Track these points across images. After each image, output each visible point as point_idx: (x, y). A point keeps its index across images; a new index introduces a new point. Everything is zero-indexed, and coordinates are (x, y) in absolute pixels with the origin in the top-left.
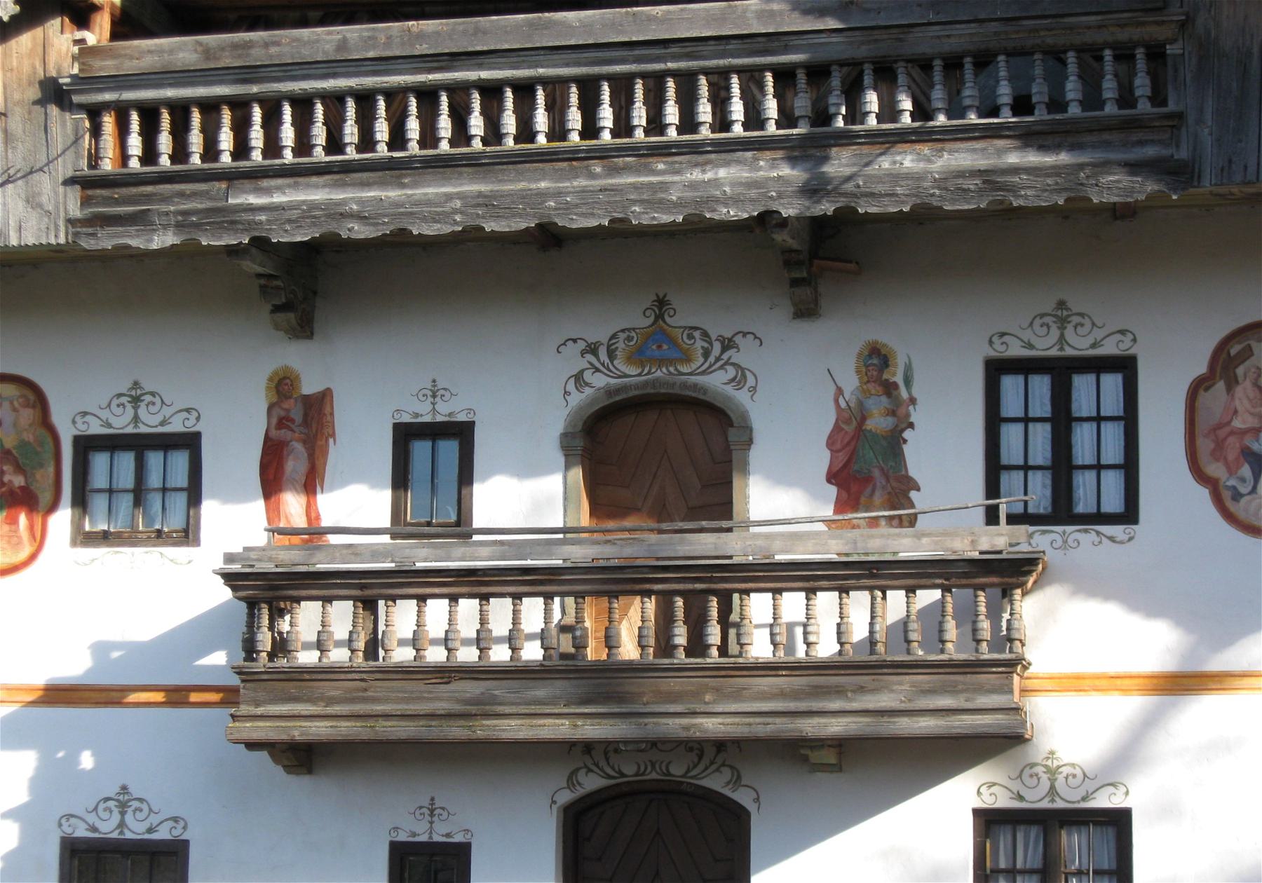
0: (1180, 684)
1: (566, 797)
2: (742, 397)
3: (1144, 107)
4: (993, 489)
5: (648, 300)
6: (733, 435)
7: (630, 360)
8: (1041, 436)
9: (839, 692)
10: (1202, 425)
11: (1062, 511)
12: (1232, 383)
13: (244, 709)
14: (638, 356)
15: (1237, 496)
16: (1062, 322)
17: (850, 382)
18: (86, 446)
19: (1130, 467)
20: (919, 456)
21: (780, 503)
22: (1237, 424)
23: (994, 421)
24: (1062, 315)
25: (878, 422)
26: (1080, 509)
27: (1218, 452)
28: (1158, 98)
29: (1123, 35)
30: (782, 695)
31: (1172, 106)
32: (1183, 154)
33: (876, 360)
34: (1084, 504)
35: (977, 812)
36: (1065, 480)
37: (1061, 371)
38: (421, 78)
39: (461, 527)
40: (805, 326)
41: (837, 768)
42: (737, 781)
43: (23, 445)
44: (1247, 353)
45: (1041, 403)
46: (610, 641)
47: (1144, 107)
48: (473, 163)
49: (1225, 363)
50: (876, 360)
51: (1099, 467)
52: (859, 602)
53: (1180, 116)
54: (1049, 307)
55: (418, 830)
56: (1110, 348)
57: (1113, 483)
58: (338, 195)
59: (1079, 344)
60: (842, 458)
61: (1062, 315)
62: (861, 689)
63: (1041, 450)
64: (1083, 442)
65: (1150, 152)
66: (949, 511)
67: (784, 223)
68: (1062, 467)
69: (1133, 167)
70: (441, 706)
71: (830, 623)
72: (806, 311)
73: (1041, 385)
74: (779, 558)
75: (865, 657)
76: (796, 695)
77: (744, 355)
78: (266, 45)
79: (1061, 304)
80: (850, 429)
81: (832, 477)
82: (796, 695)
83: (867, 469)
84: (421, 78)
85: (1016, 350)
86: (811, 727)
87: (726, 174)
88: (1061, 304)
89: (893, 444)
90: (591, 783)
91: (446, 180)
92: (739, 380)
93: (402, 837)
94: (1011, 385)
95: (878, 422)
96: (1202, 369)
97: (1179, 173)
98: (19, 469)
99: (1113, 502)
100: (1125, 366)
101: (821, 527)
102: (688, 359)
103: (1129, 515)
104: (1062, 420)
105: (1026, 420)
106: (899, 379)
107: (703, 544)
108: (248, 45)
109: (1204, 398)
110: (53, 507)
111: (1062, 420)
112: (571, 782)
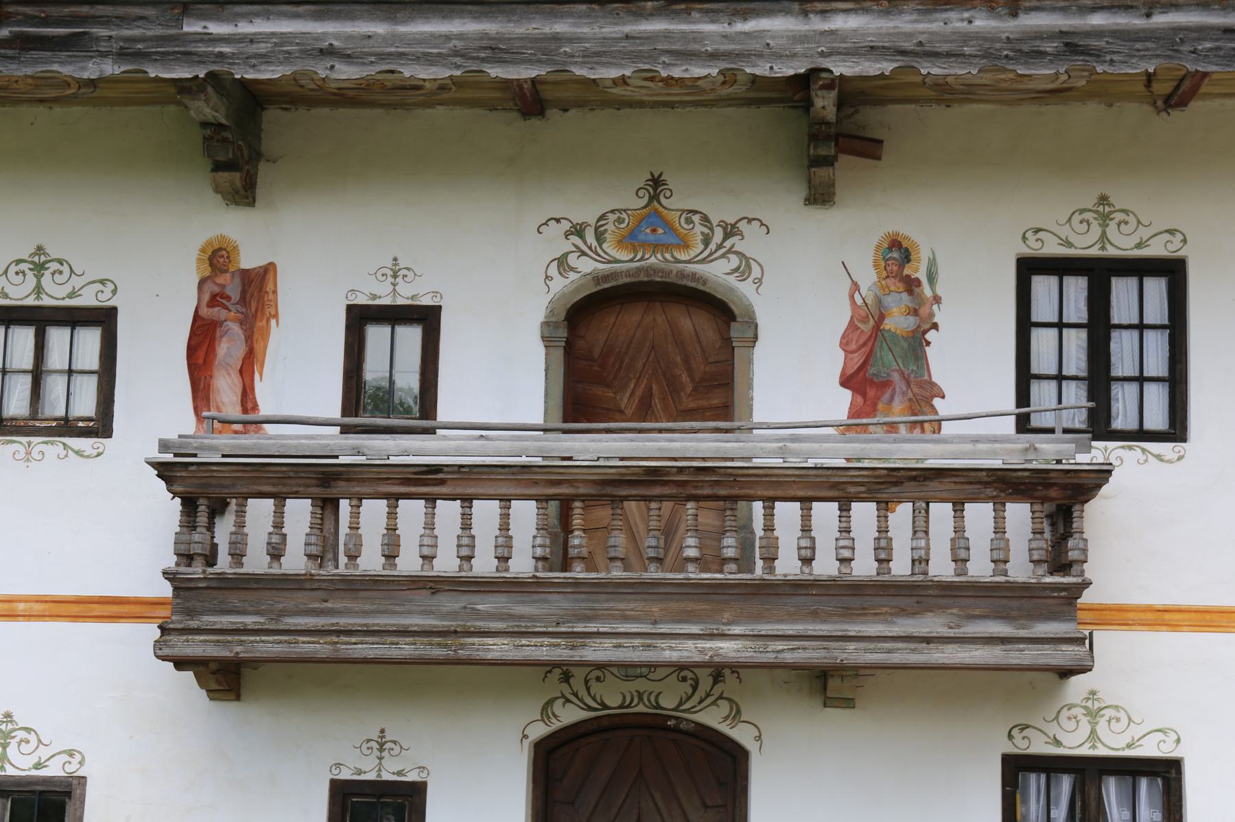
1: (539, 731)
2: (746, 289)
6: (735, 331)
7: (621, 243)
8: (1076, 342)
11: (1099, 425)
14: (630, 240)
17: (868, 277)
20: (944, 359)
23: (1025, 325)
25: (898, 322)
26: (1118, 424)
33: (897, 253)
37: (1099, 273)
40: (818, 214)
42: (735, 716)
50: (897, 253)
54: (1090, 202)
55: (367, 768)
57: (1157, 398)
59: (1123, 245)
60: (857, 359)
61: (1104, 209)
64: (1122, 348)
68: (1099, 379)
72: (820, 196)
73: (1077, 288)
77: (751, 242)
79: (1103, 200)
80: (866, 328)
85: (1052, 248)
88: (1103, 200)
89: (916, 344)
90: (569, 715)
92: (743, 271)
93: (346, 775)
102: (686, 246)
103: (1177, 430)
106: (922, 275)
112: (546, 712)
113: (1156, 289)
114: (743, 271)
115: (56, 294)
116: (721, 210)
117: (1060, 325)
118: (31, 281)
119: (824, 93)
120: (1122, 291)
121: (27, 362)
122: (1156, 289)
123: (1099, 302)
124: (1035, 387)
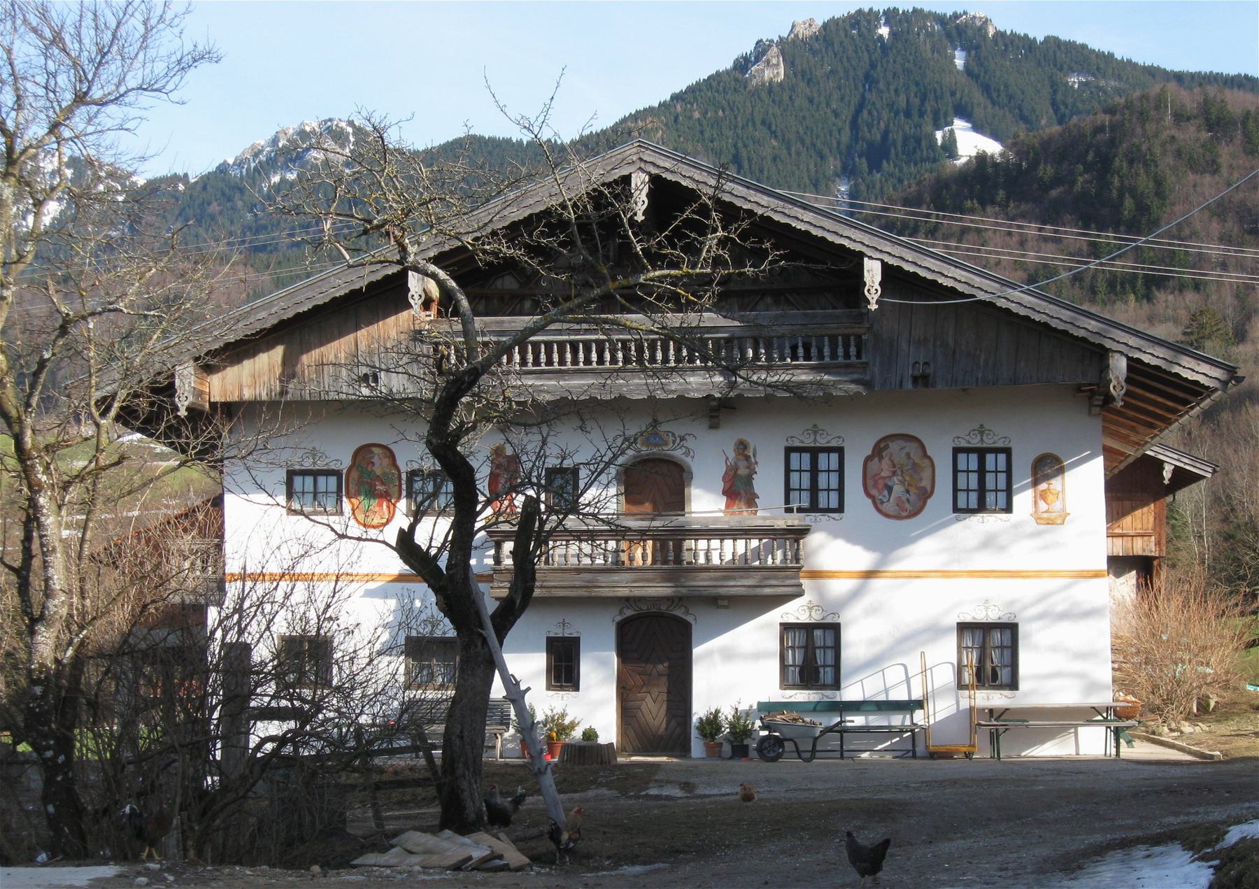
0: (869, 574)
1: (619, 618)
2: (688, 460)
3: (853, 359)
4: (787, 501)
5: (650, 420)
6: (685, 475)
7: (643, 444)
8: (806, 477)
9: (733, 578)
10: (869, 476)
11: (814, 508)
12: (881, 458)
13: (496, 584)
14: (647, 443)
15: (882, 503)
16: (815, 433)
17: (732, 455)
18: (412, 474)
19: (841, 490)
20: (759, 484)
21: (705, 503)
22: (883, 474)
23: (788, 471)
24: (815, 430)
25: (743, 471)
26: (821, 506)
27: (875, 485)
28: (859, 356)
29: (846, 332)
30: (711, 579)
31: (864, 360)
32: (868, 378)
33: (742, 446)
34: (822, 504)
35: (781, 624)
36: (817, 497)
37: (814, 452)
38: (572, 337)
39: (574, 508)
40: (714, 431)
41: (726, 607)
42: (687, 612)
43: (385, 474)
44: (887, 447)
45: (806, 464)
46: (631, 559)
47: (853, 359)
48: (593, 371)
49: (878, 450)
50: (742, 446)
51: (828, 490)
52: (728, 543)
53: (867, 363)
54: (810, 426)
55: (558, 632)
56: (834, 444)
57: (834, 496)
58: (538, 383)
59: (822, 442)
60: (728, 485)
61: (815, 430)
62: (742, 577)
63: (806, 483)
64: (822, 480)
65: (855, 376)
66: (770, 510)
67: (715, 399)
68: (814, 490)
69: (853, 382)
70: (577, 583)
71: (725, 551)
72: (714, 427)
73: (806, 457)
74: (712, 527)
75: (742, 565)
76: (716, 579)
77: (690, 443)
78: (510, 322)
79: (815, 426)
80: (732, 473)
81: (725, 493)
82: (716, 579)
83: (738, 488)
84: (572, 337)
85: (797, 444)
86: (722, 591)
87: (694, 380)
88: (815, 426)
89: (749, 480)
90: (629, 613)
91: (582, 378)
92: (687, 453)
93: (552, 635)
94: (794, 457)
95: (743, 471)
96: (870, 453)
97: (868, 384)
98: (383, 484)
99: (834, 504)
100: (840, 451)
101: (721, 514)
102: (666, 444)
103: (840, 509)
104: (814, 471)
105: (800, 471)
106: (751, 454)
107: (678, 521)
108: (503, 322)
109: (869, 464)
110: (399, 498)
111: (814, 471)
112: (621, 613)
113: (1002, 458)
114: (687, 453)
115: (320, 465)
116: (679, 431)
117: (829, 471)
118: (979, 437)
119: (381, 382)
120: (822, 458)
121: (312, 489)
122: (1002, 458)
123: (982, 463)
124: (959, 494)
